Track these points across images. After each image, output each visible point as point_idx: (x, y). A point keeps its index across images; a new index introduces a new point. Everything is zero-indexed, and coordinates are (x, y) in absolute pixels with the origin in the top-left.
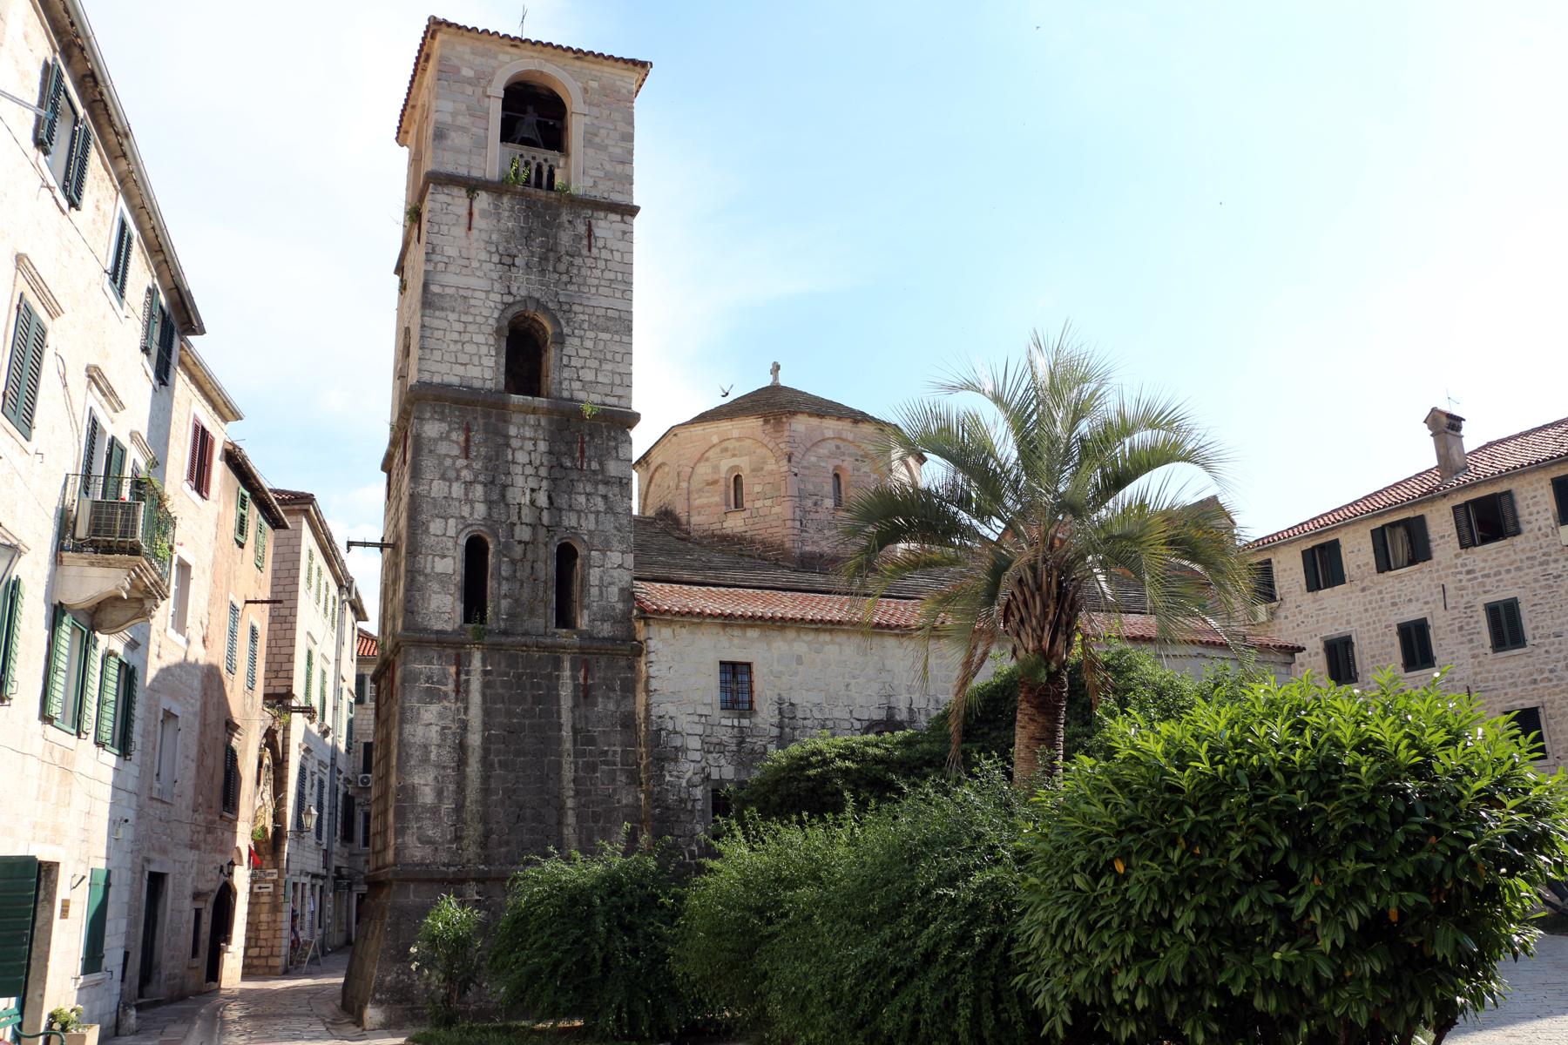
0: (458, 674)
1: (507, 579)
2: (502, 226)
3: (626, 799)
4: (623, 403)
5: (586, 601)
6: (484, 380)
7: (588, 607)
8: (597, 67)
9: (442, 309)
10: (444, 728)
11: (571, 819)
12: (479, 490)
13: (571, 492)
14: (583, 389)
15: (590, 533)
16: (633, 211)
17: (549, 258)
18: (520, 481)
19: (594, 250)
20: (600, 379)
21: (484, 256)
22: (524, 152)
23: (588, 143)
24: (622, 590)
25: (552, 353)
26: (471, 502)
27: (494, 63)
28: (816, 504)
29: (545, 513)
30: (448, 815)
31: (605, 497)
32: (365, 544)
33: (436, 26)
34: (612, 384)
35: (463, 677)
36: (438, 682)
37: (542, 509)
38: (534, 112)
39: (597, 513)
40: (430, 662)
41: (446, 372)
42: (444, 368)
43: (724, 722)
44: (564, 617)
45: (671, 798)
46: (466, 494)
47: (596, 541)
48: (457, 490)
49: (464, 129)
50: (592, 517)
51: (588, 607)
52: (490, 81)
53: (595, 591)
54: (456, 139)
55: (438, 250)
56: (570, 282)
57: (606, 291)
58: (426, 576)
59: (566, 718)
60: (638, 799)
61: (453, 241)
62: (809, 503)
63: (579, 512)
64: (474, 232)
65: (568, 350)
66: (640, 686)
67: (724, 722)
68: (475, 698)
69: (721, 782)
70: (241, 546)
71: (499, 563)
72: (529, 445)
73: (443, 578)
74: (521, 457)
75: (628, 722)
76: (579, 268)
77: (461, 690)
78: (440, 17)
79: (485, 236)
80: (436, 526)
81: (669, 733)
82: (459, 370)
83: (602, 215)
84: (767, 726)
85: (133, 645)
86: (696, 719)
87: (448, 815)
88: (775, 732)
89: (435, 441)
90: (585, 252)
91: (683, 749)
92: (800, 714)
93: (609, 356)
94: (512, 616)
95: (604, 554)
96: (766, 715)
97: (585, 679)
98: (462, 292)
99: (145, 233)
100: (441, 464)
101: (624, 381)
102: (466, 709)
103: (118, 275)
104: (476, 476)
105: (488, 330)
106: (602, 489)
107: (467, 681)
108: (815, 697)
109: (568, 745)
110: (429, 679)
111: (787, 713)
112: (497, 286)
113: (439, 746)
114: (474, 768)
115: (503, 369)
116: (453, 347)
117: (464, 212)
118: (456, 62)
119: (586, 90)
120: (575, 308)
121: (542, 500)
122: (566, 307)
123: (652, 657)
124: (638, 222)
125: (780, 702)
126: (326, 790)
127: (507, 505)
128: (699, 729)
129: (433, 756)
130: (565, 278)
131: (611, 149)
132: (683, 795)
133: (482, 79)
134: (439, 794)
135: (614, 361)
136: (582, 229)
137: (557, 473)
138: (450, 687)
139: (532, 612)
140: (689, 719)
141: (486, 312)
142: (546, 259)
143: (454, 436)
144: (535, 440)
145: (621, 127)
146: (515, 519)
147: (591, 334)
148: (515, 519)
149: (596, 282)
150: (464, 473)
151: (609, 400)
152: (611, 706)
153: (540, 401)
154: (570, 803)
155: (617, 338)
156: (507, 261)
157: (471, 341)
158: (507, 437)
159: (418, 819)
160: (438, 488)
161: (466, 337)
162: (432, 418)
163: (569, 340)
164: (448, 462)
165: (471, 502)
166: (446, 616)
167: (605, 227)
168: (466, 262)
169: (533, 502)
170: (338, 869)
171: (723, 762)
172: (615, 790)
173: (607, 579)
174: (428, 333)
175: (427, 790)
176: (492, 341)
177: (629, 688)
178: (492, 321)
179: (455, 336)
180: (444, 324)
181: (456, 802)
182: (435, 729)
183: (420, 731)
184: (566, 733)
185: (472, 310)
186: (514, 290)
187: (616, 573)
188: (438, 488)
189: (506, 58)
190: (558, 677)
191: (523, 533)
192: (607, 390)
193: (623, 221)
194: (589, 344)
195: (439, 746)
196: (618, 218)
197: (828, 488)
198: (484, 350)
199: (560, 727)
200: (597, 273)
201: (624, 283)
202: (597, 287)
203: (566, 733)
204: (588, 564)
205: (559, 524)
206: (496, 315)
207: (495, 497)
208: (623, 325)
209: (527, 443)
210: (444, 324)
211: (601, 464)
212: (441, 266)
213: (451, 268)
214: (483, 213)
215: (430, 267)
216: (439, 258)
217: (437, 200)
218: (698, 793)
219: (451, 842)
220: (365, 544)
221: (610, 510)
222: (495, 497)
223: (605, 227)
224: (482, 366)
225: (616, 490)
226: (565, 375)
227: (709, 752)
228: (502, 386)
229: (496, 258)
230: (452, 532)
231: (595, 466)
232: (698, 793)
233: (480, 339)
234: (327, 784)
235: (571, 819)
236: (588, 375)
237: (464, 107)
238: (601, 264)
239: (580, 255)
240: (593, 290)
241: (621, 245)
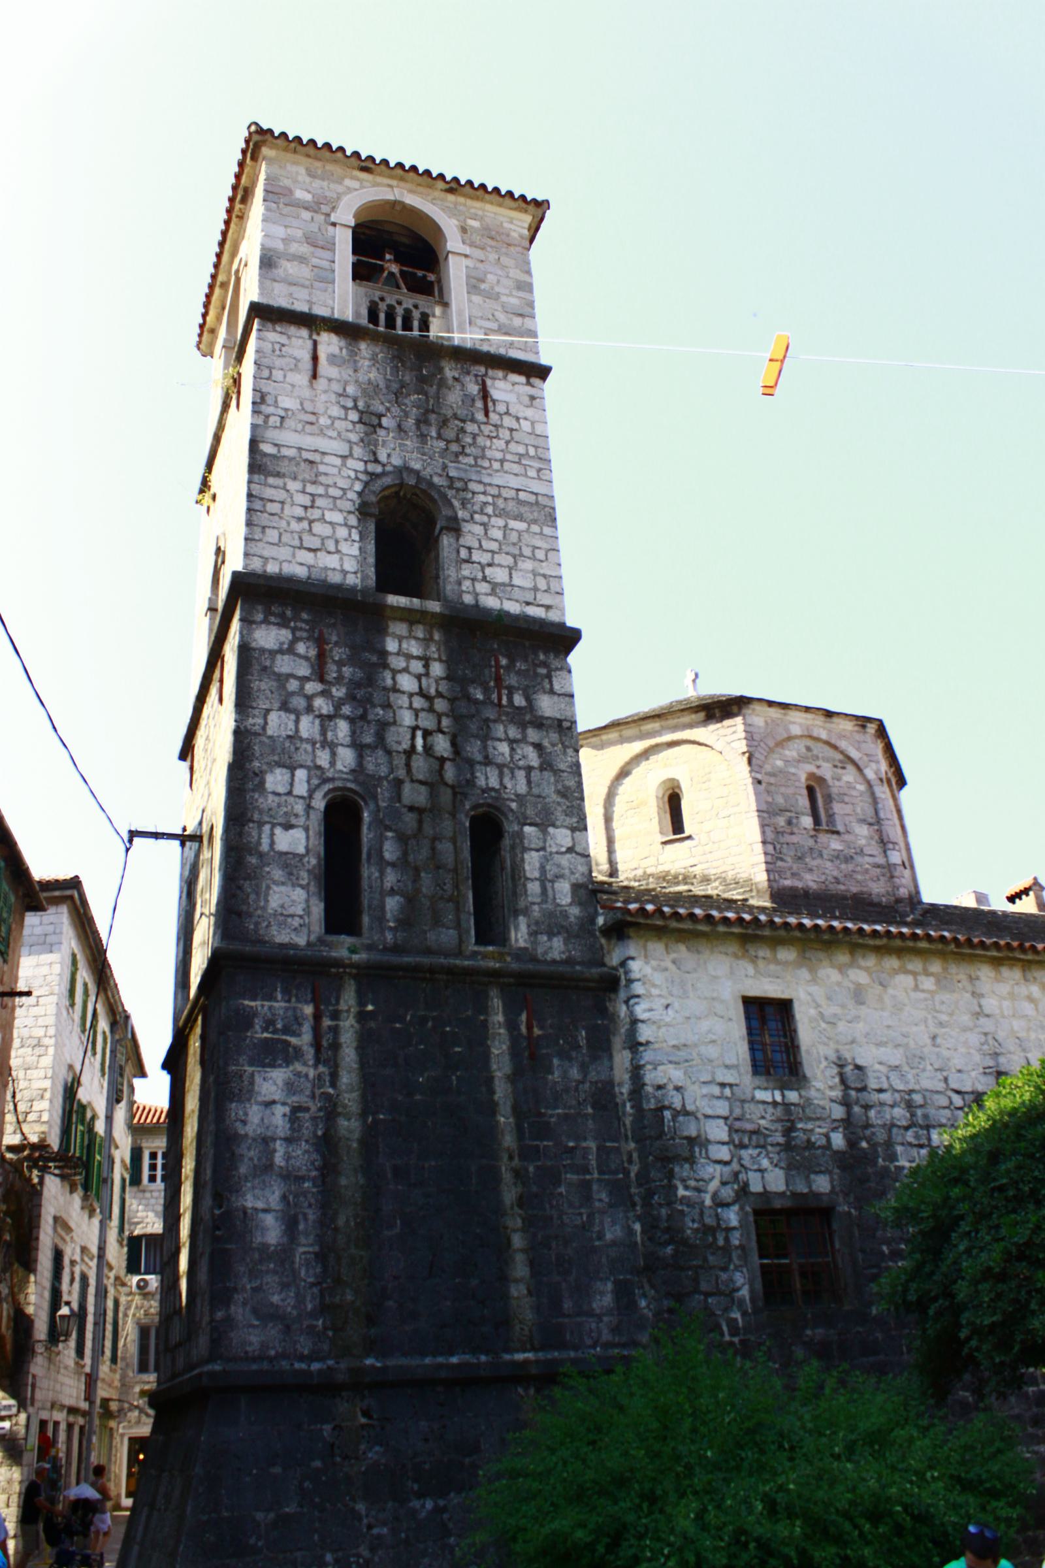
0: (317, 1017)
1: (393, 865)
2: (362, 377)
3: (613, 1233)
4: (553, 616)
5: (522, 904)
6: (345, 573)
7: (526, 912)
8: (478, 204)
9: (278, 475)
10: (296, 1110)
11: (520, 1268)
12: (342, 729)
13: (486, 737)
14: (493, 593)
15: (519, 798)
17: (431, 418)
18: (407, 718)
19: (494, 417)
20: (516, 581)
21: (336, 411)
24: (576, 887)
25: (446, 541)
26: (332, 746)
27: (340, 189)
28: (789, 823)
29: (448, 765)
30: (307, 1264)
31: (538, 747)
32: (156, 835)
33: (259, 140)
34: (535, 589)
35: (327, 1022)
36: (287, 1030)
37: (442, 760)
38: (398, 249)
39: (529, 769)
40: (271, 997)
41: (292, 563)
42: (284, 553)
43: (761, 1095)
44: (490, 928)
45: (691, 1226)
46: (323, 732)
47: (530, 812)
48: (308, 727)
49: (302, 259)
50: (521, 775)
51: (526, 912)
52: (333, 208)
53: (534, 888)
54: (289, 268)
55: (269, 400)
56: (463, 453)
57: (516, 468)
58: (261, 855)
59: (502, 1091)
60: (631, 1232)
62: (781, 821)
63: (500, 767)
64: (321, 383)
65: (467, 540)
66: (618, 1042)
67: (761, 1095)
68: (349, 1055)
69: (765, 1195)
71: (381, 839)
72: (417, 667)
73: (288, 861)
74: (407, 683)
75: (604, 1097)
76: (474, 436)
77: (326, 1050)
79: (337, 387)
80: (276, 780)
81: (676, 1114)
82: (308, 558)
83: (500, 374)
84: (825, 1103)
86: (716, 1090)
87: (307, 1264)
88: (838, 1112)
89: (273, 653)
90: (480, 416)
91: (698, 1142)
92: (873, 1084)
93: (527, 551)
94: (406, 922)
95: (545, 832)
96: (822, 1084)
97: (530, 1028)
98: (305, 455)
100: (282, 686)
101: (553, 584)
102: (334, 1077)
104: (338, 706)
105: (349, 506)
106: (533, 735)
107: (335, 1030)
108: (896, 1057)
109: (509, 1140)
110: (269, 1024)
111: (851, 1079)
112: (358, 451)
113: (288, 1140)
114: (348, 1180)
115: (371, 560)
116: (295, 526)
117: (306, 356)
118: (287, 182)
119: (464, 230)
120: (473, 486)
121: (442, 745)
122: (459, 485)
123: (638, 988)
125: (841, 1064)
126: (92, 1290)
127: (389, 752)
128: (722, 1108)
129: (279, 1159)
130: (454, 447)
131: (504, 299)
132: (709, 1221)
133: (321, 206)
134: (290, 1224)
135: (533, 558)
136: (474, 389)
137: (463, 708)
138: (304, 1039)
139: (437, 922)
140: (705, 1090)
141: (343, 483)
142: (427, 422)
143: (301, 648)
144: (426, 661)
145: (516, 274)
146: (401, 773)
147: (500, 522)
148: (401, 773)
149: (499, 455)
150: (319, 702)
151: (532, 611)
152: (575, 1073)
153: (434, 606)
154: (517, 1241)
155: (535, 528)
156: (370, 422)
157: (322, 519)
158: (384, 654)
159: (253, 1274)
160: (277, 724)
161: (316, 514)
162: (266, 621)
163: (466, 527)
164: (293, 685)
165: (332, 746)
166: (296, 922)
168: (312, 418)
169: (428, 749)
170: (105, 1402)
171: (765, 1163)
172: (591, 1216)
173: (551, 870)
174: (258, 505)
175: (269, 1220)
176: (353, 520)
177: (601, 1046)
178: (352, 495)
179: (299, 512)
180: (280, 495)
181: (320, 1239)
182: (280, 1110)
183: (254, 1114)
184: (504, 1119)
185: (322, 479)
186: (383, 457)
187: (565, 860)
188: (277, 724)
189: (355, 184)
190: (485, 1025)
191: (414, 794)
192: (529, 597)
193: (529, 383)
194: (497, 534)
195: (288, 1140)
196: (522, 379)
197: (804, 802)
198: (342, 532)
199: (491, 1109)
200: (500, 444)
201: (539, 459)
202: (502, 461)
203: (504, 1119)
204: (519, 845)
205: (471, 783)
206: (358, 487)
207: (368, 739)
208: (544, 513)
209: (411, 662)
210: (280, 495)
211: (528, 699)
212: (274, 421)
213: (289, 423)
214: (332, 359)
215: (260, 421)
216: (271, 410)
218: (732, 1217)
219: (313, 1315)
220: (156, 835)
221: (547, 765)
222: (368, 739)
224: (341, 555)
225: (554, 736)
226: (466, 573)
227: (742, 1146)
228: (372, 581)
230: (301, 789)
231: (519, 700)
232: (732, 1217)
233: (337, 517)
234: (92, 1281)
235: (520, 1268)
236: (500, 575)
237: (299, 233)
238: (505, 434)
239: (473, 420)
240: (496, 465)
241: (529, 412)
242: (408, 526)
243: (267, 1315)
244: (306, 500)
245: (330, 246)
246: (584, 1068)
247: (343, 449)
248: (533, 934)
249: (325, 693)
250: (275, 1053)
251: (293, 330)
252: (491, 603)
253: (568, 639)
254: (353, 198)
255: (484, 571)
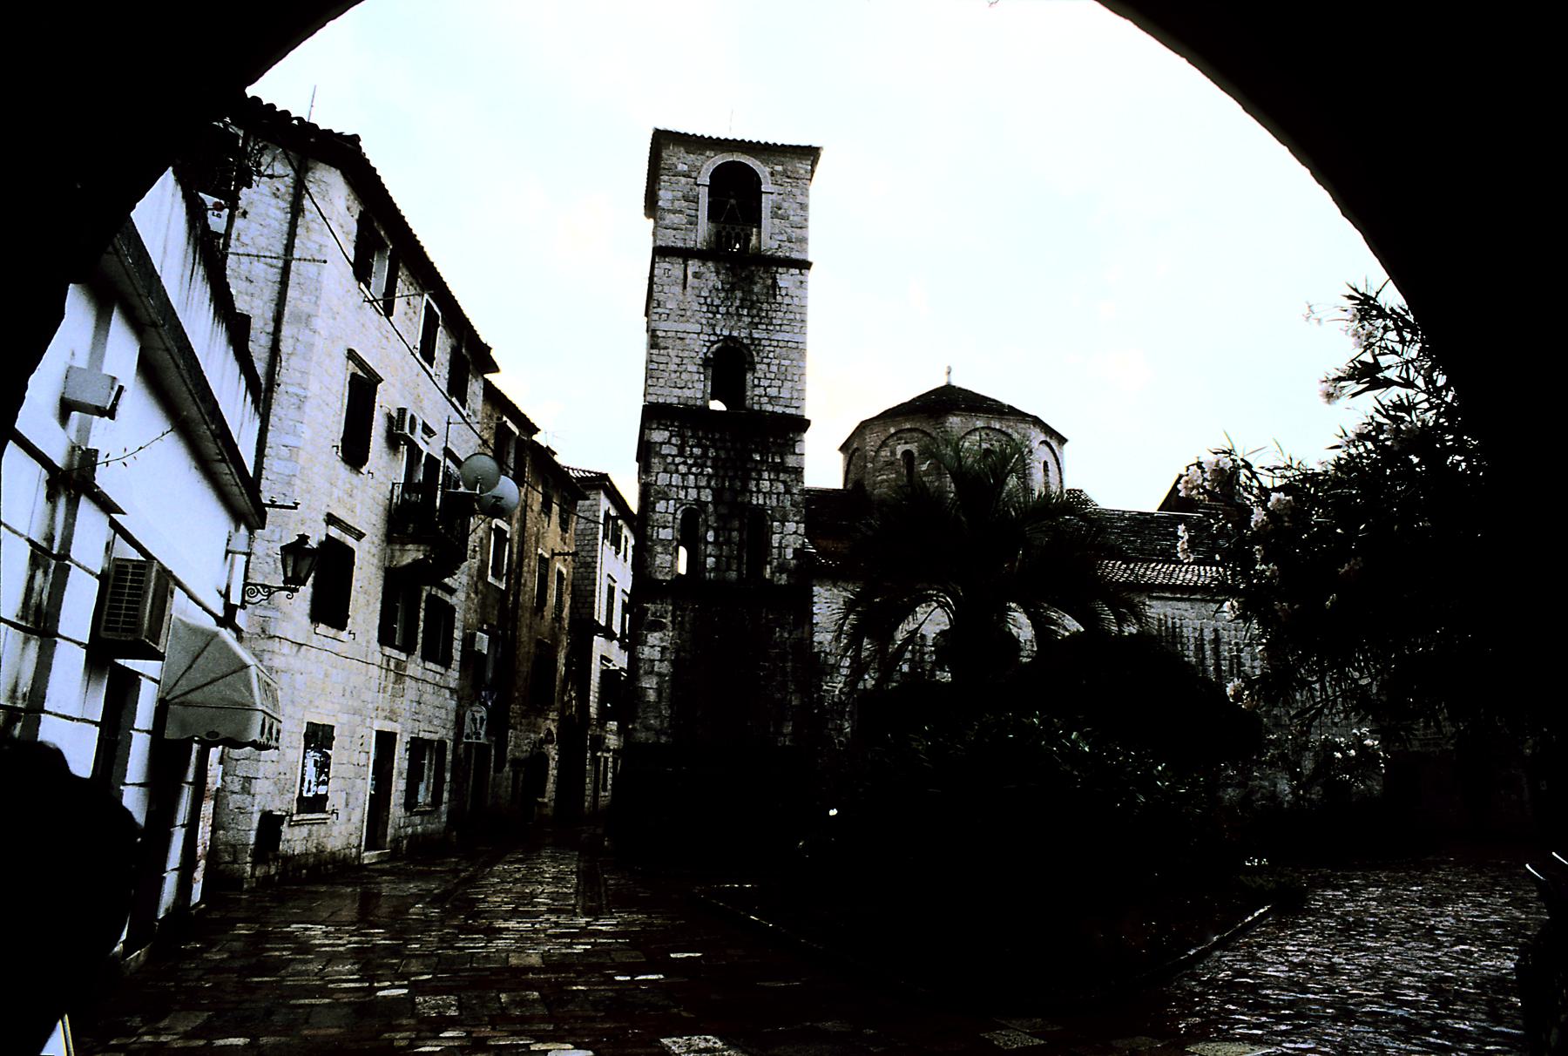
4: (799, 412)
15: (772, 508)
16: (805, 265)
22: (728, 217)
23: (775, 215)
24: (795, 550)
26: (686, 488)
31: (784, 482)
33: (663, 140)
41: (671, 397)
42: (666, 391)
48: (676, 479)
53: (775, 551)
61: (671, 297)
65: (759, 374)
70: (603, 658)
78: (661, 128)
80: (661, 506)
81: (827, 654)
82: (677, 392)
85: (392, 557)
99: (447, 314)
103: (427, 352)
124: (812, 275)
134: (659, 691)
143: (674, 440)
151: (788, 411)
160: (663, 479)
164: (669, 460)
165: (686, 488)
167: (786, 279)
179: (674, 367)
187: (791, 539)
217: (662, 266)
223: (786, 279)
224: (693, 388)
229: (705, 309)
230: (671, 510)
236: (773, 392)
238: (784, 308)
241: (798, 292)
242: (730, 365)
243: (648, 728)
244: (678, 361)
245: (696, 200)
246: (790, 633)
247: (697, 328)
248: (773, 573)
249: (685, 463)
250: (657, 626)
251: (674, 259)
252: (769, 408)
253: (802, 424)
254: (710, 163)
255: (762, 392)
